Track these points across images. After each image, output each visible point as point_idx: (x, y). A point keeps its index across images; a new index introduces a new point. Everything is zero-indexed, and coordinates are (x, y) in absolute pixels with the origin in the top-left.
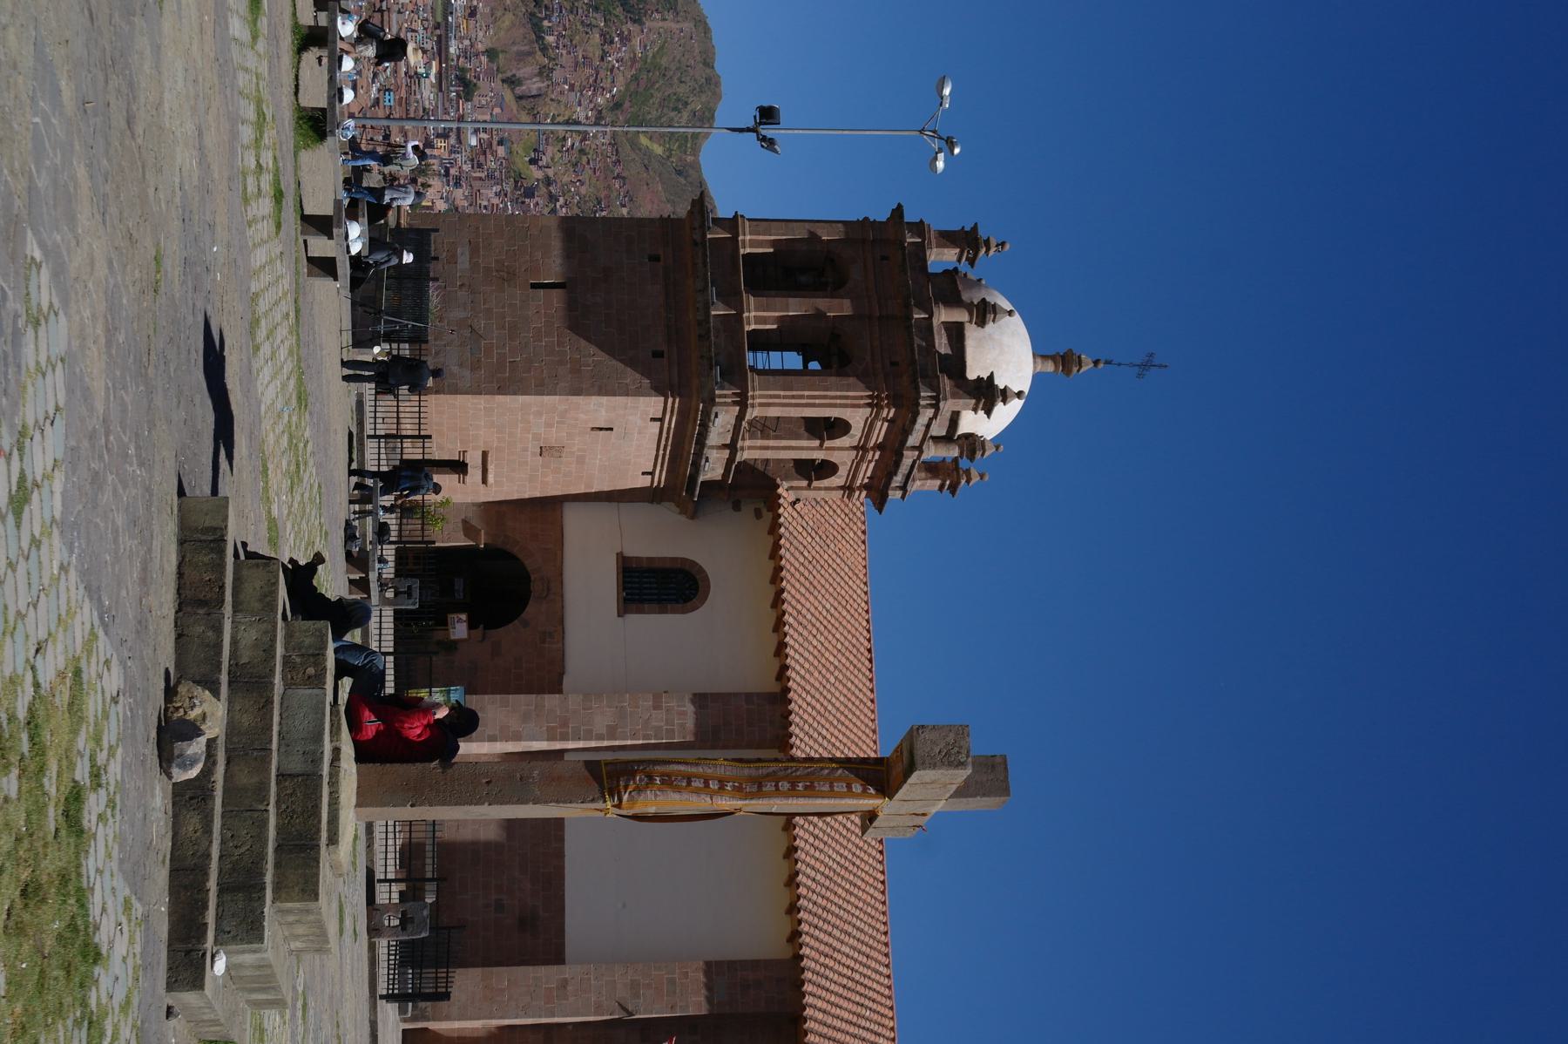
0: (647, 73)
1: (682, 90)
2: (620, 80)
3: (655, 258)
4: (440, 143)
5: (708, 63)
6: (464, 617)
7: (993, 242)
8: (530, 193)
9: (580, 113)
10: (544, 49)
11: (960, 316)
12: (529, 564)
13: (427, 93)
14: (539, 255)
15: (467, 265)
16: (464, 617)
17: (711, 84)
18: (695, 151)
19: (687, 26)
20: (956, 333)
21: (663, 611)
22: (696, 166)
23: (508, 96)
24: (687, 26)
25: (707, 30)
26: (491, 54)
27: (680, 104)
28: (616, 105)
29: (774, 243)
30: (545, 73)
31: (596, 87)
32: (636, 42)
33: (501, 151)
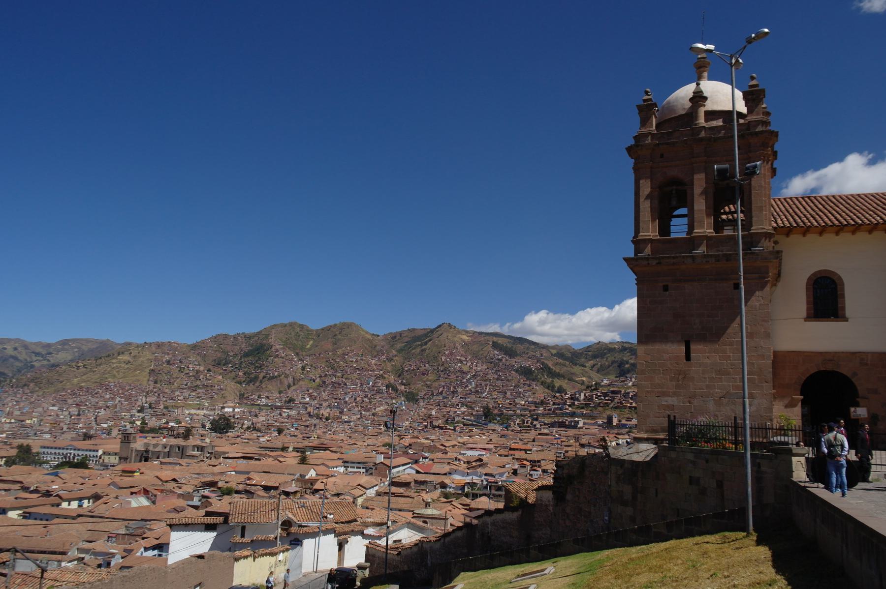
0: (287, 344)
1: (293, 334)
2: (290, 353)
3: (666, 288)
4: (309, 410)
5: (285, 325)
6: (852, 409)
7: (646, 97)
8: (324, 382)
9: (300, 366)
10: (279, 376)
11: (701, 111)
12: (815, 370)
13: (293, 413)
14: (666, 356)
15: (675, 399)
16: (852, 409)
17: (292, 325)
18: (312, 331)
19: (273, 331)
20: (711, 115)
21: (843, 296)
22: (317, 331)
23: (293, 388)
24: (273, 331)
25: (275, 325)
26: (280, 392)
27: (298, 335)
28: (297, 354)
29: (653, 220)
30: (287, 376)
31: (291, 360)
32: (278, 347)
33: (311, 391)
